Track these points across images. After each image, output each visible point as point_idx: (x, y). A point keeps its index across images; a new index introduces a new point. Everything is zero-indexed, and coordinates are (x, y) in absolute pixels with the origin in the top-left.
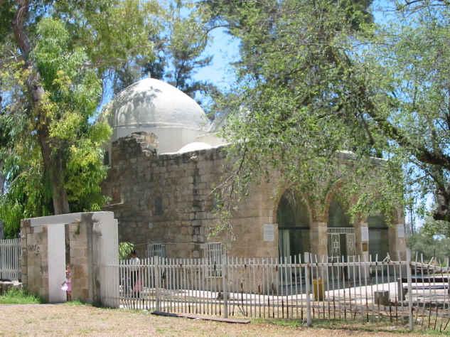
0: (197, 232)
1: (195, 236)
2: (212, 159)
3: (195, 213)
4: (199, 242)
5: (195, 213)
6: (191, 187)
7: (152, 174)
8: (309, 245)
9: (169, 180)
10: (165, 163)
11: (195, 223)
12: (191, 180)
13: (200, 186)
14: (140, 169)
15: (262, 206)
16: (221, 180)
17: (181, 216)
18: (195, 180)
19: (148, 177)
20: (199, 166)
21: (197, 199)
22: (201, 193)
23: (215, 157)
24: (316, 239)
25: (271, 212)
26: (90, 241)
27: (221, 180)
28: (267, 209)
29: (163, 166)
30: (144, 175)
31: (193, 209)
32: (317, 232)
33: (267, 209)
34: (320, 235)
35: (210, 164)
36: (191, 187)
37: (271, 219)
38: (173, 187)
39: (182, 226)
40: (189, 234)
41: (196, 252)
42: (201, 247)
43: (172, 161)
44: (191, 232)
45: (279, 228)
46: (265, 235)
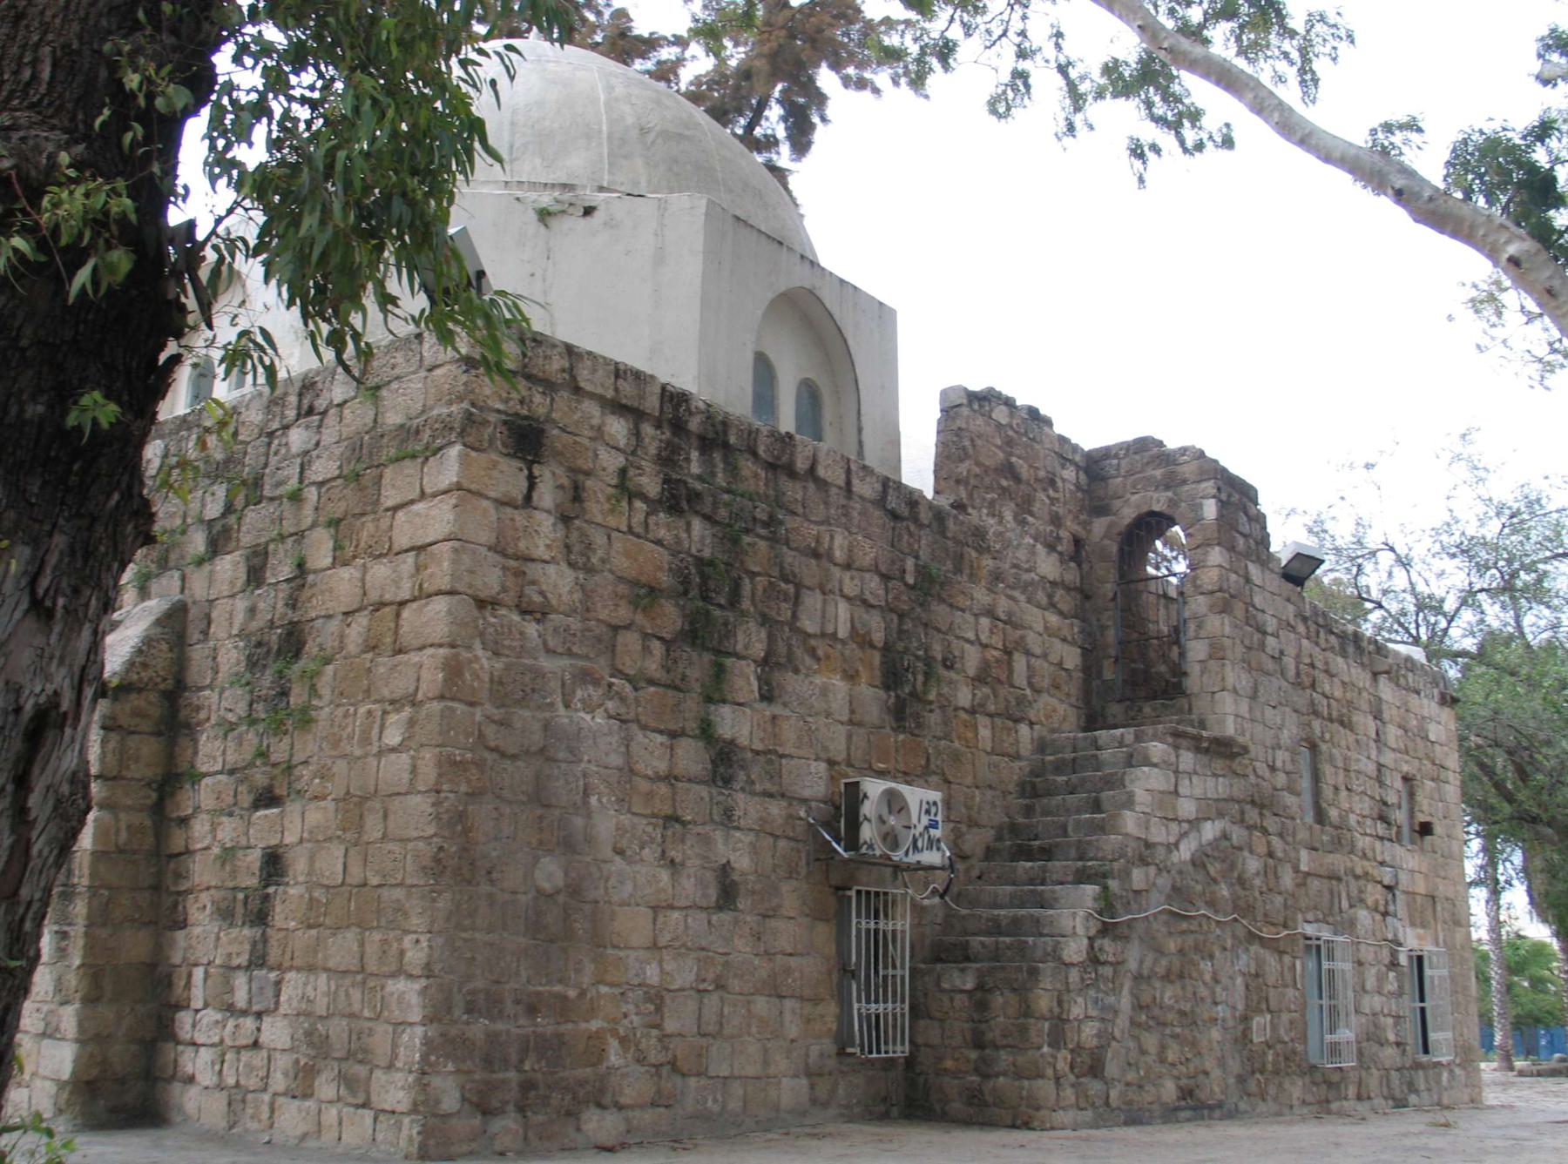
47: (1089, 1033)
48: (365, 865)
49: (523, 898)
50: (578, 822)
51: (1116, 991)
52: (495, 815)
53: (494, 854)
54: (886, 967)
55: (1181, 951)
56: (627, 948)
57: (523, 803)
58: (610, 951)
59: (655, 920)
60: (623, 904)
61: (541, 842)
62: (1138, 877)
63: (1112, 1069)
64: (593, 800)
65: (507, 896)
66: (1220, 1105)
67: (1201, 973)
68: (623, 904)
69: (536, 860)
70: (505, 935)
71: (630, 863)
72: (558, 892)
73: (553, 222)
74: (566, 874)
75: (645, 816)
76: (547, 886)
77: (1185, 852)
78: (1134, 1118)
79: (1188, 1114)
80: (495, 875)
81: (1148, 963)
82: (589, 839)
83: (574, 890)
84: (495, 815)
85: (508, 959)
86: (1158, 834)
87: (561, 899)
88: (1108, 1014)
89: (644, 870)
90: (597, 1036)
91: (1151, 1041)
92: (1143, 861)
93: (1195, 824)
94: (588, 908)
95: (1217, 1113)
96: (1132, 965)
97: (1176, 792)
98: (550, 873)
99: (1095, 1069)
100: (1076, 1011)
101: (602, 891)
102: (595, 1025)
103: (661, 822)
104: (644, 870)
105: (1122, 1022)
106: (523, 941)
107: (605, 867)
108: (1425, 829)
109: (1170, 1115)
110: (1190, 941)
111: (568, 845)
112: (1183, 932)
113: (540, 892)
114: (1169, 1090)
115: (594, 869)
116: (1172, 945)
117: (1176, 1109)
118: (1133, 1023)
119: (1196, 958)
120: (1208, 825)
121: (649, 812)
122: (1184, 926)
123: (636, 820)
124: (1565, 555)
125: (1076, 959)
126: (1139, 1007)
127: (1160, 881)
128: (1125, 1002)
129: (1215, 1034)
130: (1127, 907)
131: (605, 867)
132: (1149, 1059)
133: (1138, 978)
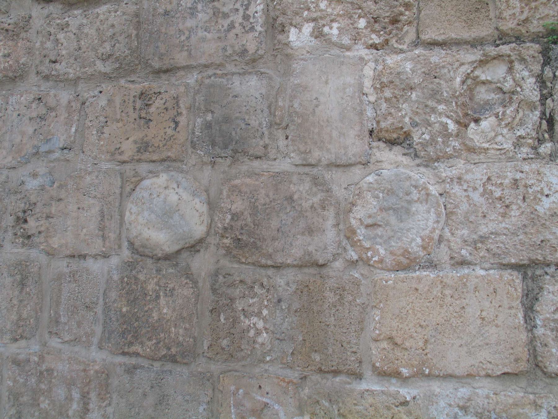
48: (46, 152)
49: (95, 266)
50: (250, 88)
52: (37, 110)
53: (32, 184)
56: (419, 375)
57: (107, 77)
58: (370, 384)
59: (530, 302)
60: (407, 263)
61: (144, 147)
64: (299, 37)
65: (61, 265)
68: (407, 263)
69: (130, 186)
70: (55, 343)
71: (429, 162)
72: (195, 247)
74: (212, 206)
75: (475, 43)
76: (161, 239)
80: (32, 225)
82: (290, 122)
83: (242, 240)
84: (37, 110)
85: (61, 392)
87: (202, 264)
89: (478, 174)
94: (284, 281)
98: (172, 206)
101: (331, 235)
103: (532, 49)
104: (478, 174)
106: (98, 357)
107: (339, 182)
111: (225, 141)
113: (141, 252)
115: (301, 189)
121: (484, 30)
123: (437, 56)
124: (557, 192)
131: (339, 182)
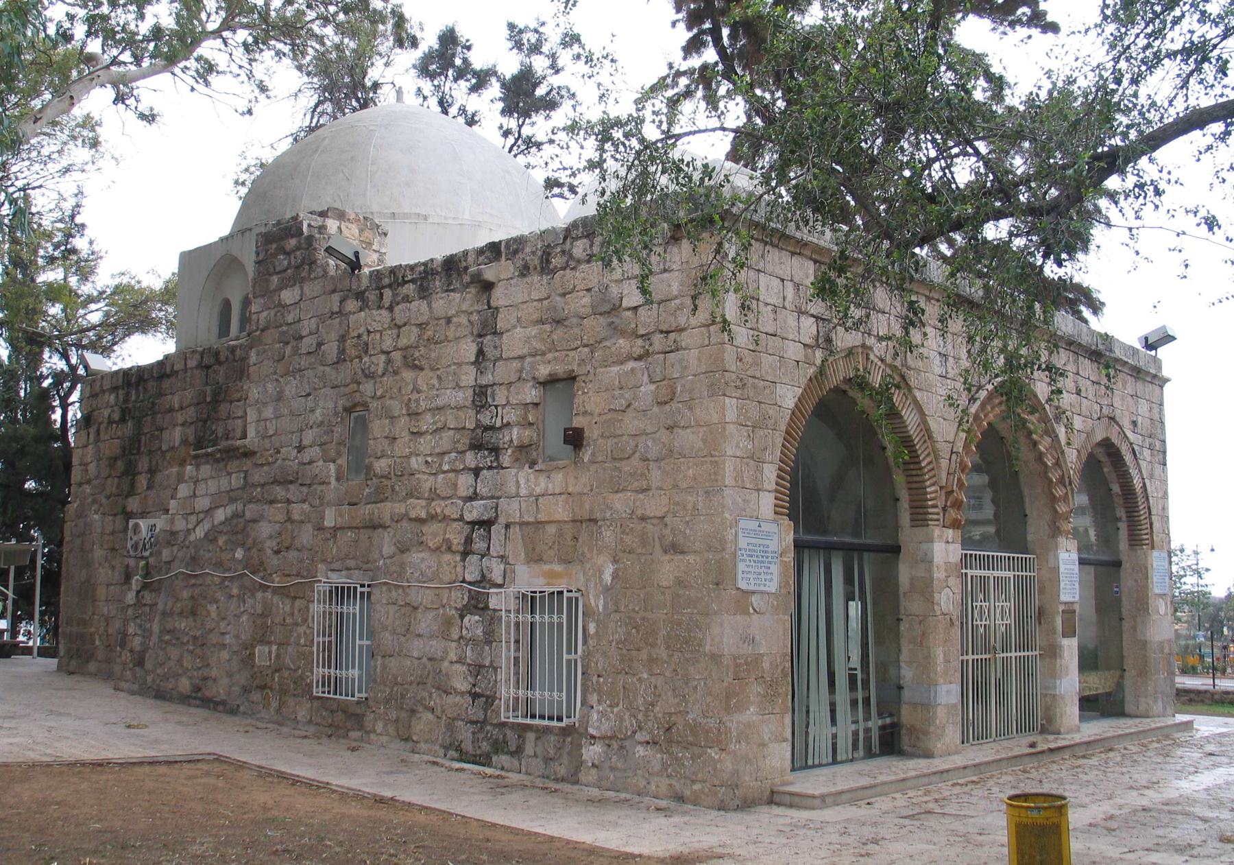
0: (479, 545)
1: (473, 559)
2: (545, 267)
3: (476, 472)
4: (484, 580)
5: (476, 472)
6: (469, 376)
7: (343, 339)
8: (897, 607)
9: (397, 356)
10: (388, 293)
11: (475, 511)
12: (469, 350)
13: (501, 372)
14: (307, 326)
15: (735, 445)
16: (273, 287)
17: (427, 483)
18: (480, 352)
19: (331, 349)
20: (499, 297)
21: (485, 419)
22: (500, 400)
23: (557, 261)
24: (925, 588)
25: (770, 474)
26: (787, 799)
27: (273, 287)
28: (756, 458)
29: (379, 308)
30: (320, 345)
31: (470, 459)
32: (928, 561)
33: (756, 458)
34: (939, 574)
35: (537, 285)
36: (469, 376)
37: (767, 502)
38: (408, 375)
39: (432, 517)
40: (449, 549)
41: (471, 619)
42: (493, 603)
43: (410, 289)
44: (457, 541)
45: (799, 546)
46: (741, 567)
47: (137, 642)
51: (151, 621)
54: (330, 642)
55: (192, 597)
62: (166, 554)
63: (149, 665)
66: (223, 703)
67: (209, 613)
73: (415, 604)
77: (200, 533)
78: (160, 695)
79: (198, 702)
81: (170, 604)
86: (180, 525)
88: (146, 634)
90: (91, 634)
91: (174, 653)
92: (169, 544)
93: (209, 512)
95: (221, 708)
96: (160, 606)
97: (195, 495)
99: (140, 662)
100: (131, 630)
102: (93, 630)
105: (155, 638)
108: (573, 95)
109: (185, 699)
110: (197, 591)
112: (194, 585)
114: (185, 685)
116: (185, 594)
117: (188, 697)
118: (161, 641)
119: (204, 602)
120: (221, 510)
122: (193, 581)
125: (131, 602)
126: (164, 631)
127: (180, 555)
128: (156, 627)
129: (225, 655)
130: (159, 572)
132: (172, 663)
133: (164, 614)
